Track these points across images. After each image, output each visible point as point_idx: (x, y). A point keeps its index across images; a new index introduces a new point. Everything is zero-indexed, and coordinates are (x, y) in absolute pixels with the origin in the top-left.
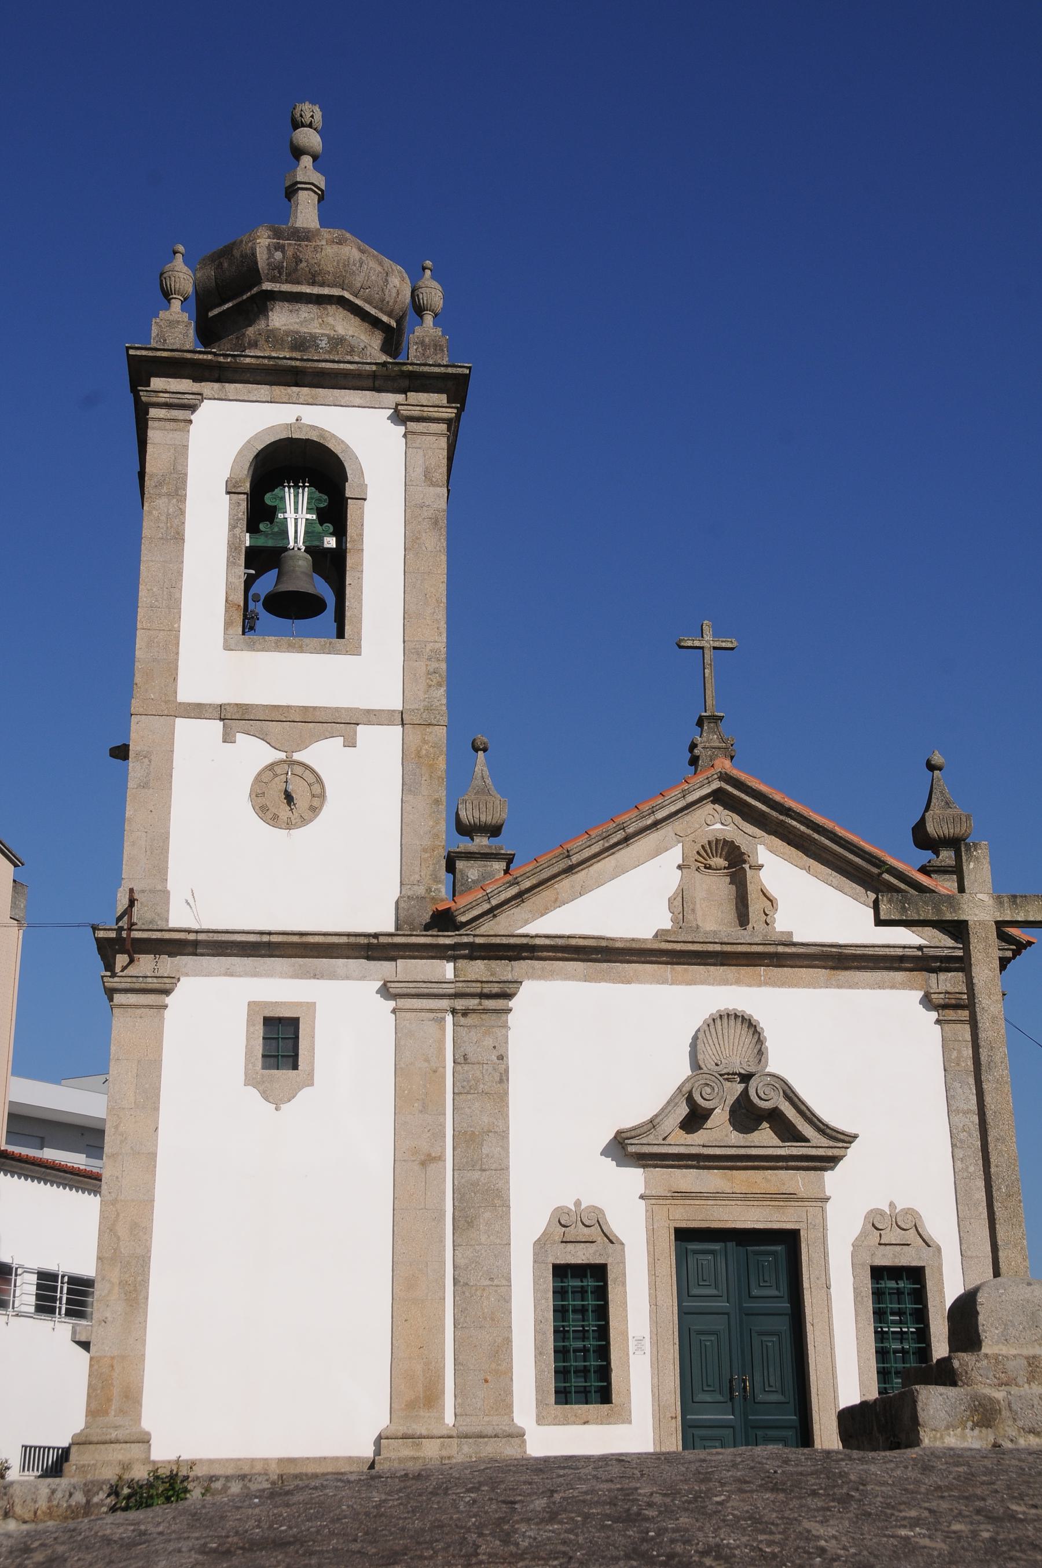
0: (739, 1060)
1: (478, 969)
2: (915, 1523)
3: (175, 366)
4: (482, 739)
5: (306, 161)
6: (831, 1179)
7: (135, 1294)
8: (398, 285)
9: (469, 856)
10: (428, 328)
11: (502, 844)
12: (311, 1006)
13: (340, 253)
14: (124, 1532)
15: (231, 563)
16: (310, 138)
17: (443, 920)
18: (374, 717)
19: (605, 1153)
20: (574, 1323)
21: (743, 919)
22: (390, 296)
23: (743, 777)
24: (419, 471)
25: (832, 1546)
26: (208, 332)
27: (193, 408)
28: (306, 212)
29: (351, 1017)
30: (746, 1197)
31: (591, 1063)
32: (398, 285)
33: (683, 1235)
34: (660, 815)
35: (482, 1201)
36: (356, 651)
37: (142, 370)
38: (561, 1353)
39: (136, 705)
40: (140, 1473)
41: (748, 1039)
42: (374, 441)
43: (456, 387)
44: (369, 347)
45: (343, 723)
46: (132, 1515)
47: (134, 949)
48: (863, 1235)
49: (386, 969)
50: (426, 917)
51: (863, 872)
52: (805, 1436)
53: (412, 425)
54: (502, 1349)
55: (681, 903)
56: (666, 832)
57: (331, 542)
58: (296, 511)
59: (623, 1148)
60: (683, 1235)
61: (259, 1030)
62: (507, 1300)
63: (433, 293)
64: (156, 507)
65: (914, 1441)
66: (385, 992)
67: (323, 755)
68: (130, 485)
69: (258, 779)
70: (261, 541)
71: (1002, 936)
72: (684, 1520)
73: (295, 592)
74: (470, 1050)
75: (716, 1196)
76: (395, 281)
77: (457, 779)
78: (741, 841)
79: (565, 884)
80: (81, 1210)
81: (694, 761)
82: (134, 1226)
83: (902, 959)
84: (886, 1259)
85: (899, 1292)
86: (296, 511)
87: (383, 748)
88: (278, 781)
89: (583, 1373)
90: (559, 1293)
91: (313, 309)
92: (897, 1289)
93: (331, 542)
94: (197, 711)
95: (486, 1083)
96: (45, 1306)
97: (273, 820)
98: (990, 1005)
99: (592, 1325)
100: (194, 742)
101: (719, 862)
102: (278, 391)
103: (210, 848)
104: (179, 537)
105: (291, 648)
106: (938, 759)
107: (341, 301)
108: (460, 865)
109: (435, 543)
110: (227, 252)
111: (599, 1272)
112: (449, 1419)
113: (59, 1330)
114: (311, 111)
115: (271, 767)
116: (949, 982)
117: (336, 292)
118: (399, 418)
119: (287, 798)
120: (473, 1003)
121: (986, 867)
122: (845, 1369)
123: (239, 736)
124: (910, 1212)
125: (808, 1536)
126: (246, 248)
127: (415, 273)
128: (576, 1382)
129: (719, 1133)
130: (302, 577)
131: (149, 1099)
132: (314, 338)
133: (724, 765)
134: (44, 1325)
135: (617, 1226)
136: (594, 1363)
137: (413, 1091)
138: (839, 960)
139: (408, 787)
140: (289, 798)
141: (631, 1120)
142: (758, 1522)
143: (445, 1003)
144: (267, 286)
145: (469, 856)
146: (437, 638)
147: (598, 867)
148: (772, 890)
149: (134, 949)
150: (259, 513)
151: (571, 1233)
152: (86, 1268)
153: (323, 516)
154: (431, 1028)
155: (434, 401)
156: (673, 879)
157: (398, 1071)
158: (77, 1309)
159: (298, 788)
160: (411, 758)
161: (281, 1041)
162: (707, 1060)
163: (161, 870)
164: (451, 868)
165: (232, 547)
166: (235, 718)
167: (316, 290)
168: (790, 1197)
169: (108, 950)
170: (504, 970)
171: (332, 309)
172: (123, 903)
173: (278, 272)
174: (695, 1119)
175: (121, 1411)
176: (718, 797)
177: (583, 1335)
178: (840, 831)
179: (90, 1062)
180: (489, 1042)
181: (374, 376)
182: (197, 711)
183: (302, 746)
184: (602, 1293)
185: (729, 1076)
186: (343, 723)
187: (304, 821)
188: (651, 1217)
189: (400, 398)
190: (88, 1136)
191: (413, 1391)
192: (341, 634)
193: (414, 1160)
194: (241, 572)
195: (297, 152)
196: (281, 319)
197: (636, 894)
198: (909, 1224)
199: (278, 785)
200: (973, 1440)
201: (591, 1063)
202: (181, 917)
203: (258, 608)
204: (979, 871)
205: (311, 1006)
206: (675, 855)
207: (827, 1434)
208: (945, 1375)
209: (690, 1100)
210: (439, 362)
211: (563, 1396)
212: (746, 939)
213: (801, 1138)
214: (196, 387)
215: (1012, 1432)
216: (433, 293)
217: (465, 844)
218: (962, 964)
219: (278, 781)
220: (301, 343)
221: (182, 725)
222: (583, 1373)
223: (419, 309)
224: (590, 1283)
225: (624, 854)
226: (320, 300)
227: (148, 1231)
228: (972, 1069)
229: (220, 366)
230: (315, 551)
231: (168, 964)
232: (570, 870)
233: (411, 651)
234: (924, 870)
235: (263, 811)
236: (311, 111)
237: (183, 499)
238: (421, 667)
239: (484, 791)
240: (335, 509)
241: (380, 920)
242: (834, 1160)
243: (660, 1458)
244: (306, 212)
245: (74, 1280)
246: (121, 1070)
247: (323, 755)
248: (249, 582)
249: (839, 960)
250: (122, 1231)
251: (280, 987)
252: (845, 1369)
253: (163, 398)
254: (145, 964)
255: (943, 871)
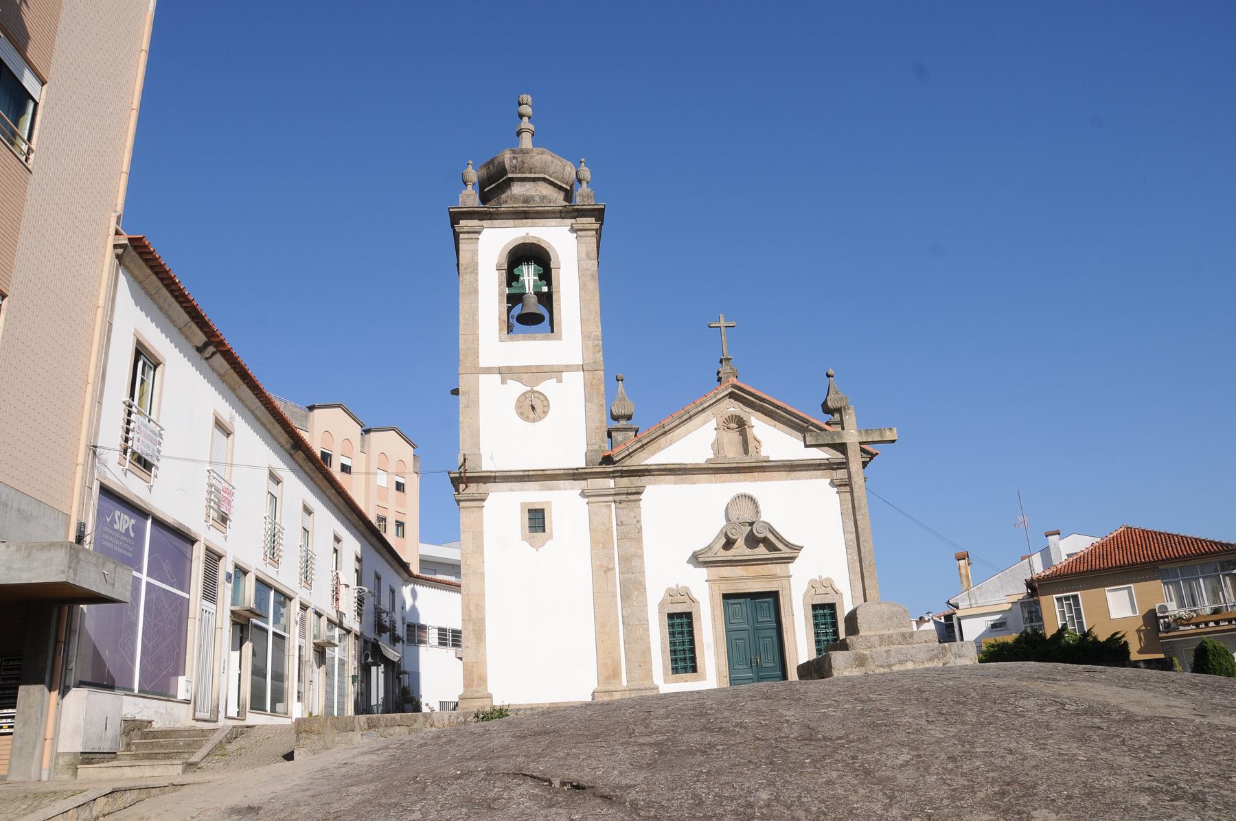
0: (747, 516)
1: (625, 481)
2: (829, 706)
3: (470, 215)
4: (621, 375)
5: (525, 119)
6: (792, 567)
7: (480, 635)
8: (570, 171)
9: (618, 430)
10: (584, 189)
11: (633, 423)
12: (549, 503)
13: (544, 159)
14: (481, 730)
15: (500, 302)
16: (526, 109)
17: (608, 460)
18: (569, 368)
19: (688, 562)
20: (678, 638)
21: (746, 451)
22: (566, 175)
23: (742, 385)
24: (584, 254)
25: (792, 719)
26: (485, 198)
27: (479, 233)
28: (526, 141)
29: (568, 507)
30: (754, 578)
31: (680, 522)
32: (570, 171)
33: (726, 597)
34: (705, 405)
35: (633, 587)
36: (560, 338)
37: (455, 218)
38: (673, 652)
39: (461, 370)
40: (488, 709)
41: (751, 506)
42: (563, 242)
43: (599, 214)
44: (558, 199)
45: (555, 372)
46: (485, 723)
47: (466, 481)
48: (808, 591)
49: (582, 484)
50: (600, 460)
51: (800, 426)
52: (784, 676)
53: (591, 499)
54: (647, 651)
55: (717, 446)
56: (708, 413)
57: (545, 289)
58: (529, 275)
59: (697, 559)
60: (726, 597)
61: (527, 515)
62: (647, 630)
63: (586, 173)
64: (465, 279)
65: (829, 674)
66: (583, 494)
67: (547, 387)
68: (453, 266)
69: (518, 400)
70: (513, 291)
71: (863, 450)
72: (726, 714)
73: (530, 313)
74: (624, 519)
75: (740, 578)
76: (568, 169)
77: (610, 395)
78: (743, 415)
79: (663, 440)
80: (454, 599)
81: (719, 380)
82: (477, 605)
83: (820, 465)
84: (819, 600)
85: (825, 615)
86: (529, 275)
87: (575, 383)
88: (530, 398)
89: (684, 658)
90: (671, 626)
91: (532, 184)
92: (824, 613)
93: (545, 289)
94: (489, 371)
95: (632, 534)
96: (443, 642)
97: (527, 419)
98: (858, 480)
99: (687, 639)
100: (488, 386)
101: (734, 425)
102: (518, 221)
103: (497, 432)
104: (476, 292)
105: (530, 339)
106: (831, 372)
107: (544, 180)
108: (613, 434)
109: (593, 286)
110: (492, 162)
111: (689, 615)
112: (625, 683)
113: (449, 652)
114: (526, 98)
115: (524, 394)
116: (841, 474)
117: (541, 176)
118: (573, 230)
119: (532, 408)
120: (624, 497)
121: (854, 418)
122: (801, 646)
123: (509, 381)
124: (828, 579)
125: (781, 716)
126: (500, 160)
127: (577, 164)
128: (681, 664)
129: (740, 550)
130: (532, 306)
131: (479, 549)
132: (532, 197)
133: (733, 380)
134: (443, 650)
135: (695, 594)
136: (688, 655)
137: (599, 539)
138: (792, 467)
139: (587, 400)
140: (533, 408)
141: (700, 545)
142: (758, 712)
143: (611, 498)
144: (510, 175)
145: (618, 430)
146: (597, 331)
147: (677, 431)
148: (759, 438)
149: (466, 481)
150: (512, 278)
151: (675, 599)
152: (458, 626)
153: (541, 277)
154: (605, 510)
155: (590, 222)
156: (713, 435)
157: (592, 530)
158: (457, 643)
159: (537, 404)
160: (588, 386)
161: (537, 519)
162: (733, 517)
163: (477, 445)
164: (609, 436)
165: (500, 294)
166: (506, 373)
167: (533, 176)
168: (774, 576)
169: (456, 482)
170: (637, 481)
171: (540, 183)
172: (462, 460)
173: (515, 169)
174: (729, 544)
175: (479, 685)
176: (731, 395)
177: (683, 643)
178: (789, 408)
179: (451, 535)
180: (632, 515)
181: (561, 212)
182: (489, 371)
183: (538, 383)
184: (690, 625)
185: (743, 524)
186: (555, 372)
187: (541, 418)
188: (711, 589)
189: (573, 221)
190: (454, 568)
191: (608, 672)
192: (552, 331)
193: (602, 570)
194: (505, 305)
195: (521, 116)
196: (517, 189)
197: (696, 442)
198: (829, 585)
199: (528, 403)
200: (856, 672)
201: (680, 522)
202: (488, 465)
203: (514, 321)
204: (850, 419)
205: (549, 503)
206: (713, 423)
207: (793, 675)
208: (844, 646)
209: (726, 535)
210: (590, 203)
211: (675, 670)
212: (748, 460)
213: (777, 549)
214: (480, 223)
215: (873, 668)
216: (586, 173)
217: (615, 425)
218: (844, 465)
219: (530, 398)
220: (527, 200)
221: (483, 378)
222: (684, 658)
223: (580, 181)
224: (685, 620)
225: (690, 425)
226: (534, 180)
227: (483, 607)
228: (853, 512)
229: (491, 213)
230: (539, 294)
231: (483, 487)
232: (665, 433)
233: (585, 336)
234: (827, 423)
235: (521, 414)
236: (526, 98)
237: (477, 274)
238: (590, 343)
239: (623, 399)
240: (546, 275)
241: (579, 462)
242: (793, 558)
243: (719, 690)
244: (526, 141)
245: (454, 631)
246: (466, 537)
247: (547, 387)
248: (509, 310)
249: (792, 467)
250: (472, 608)
251: (535, 495)
252: (801, 646)
253: (466, 229)
254: (473, 488)
255: (836, 423)
